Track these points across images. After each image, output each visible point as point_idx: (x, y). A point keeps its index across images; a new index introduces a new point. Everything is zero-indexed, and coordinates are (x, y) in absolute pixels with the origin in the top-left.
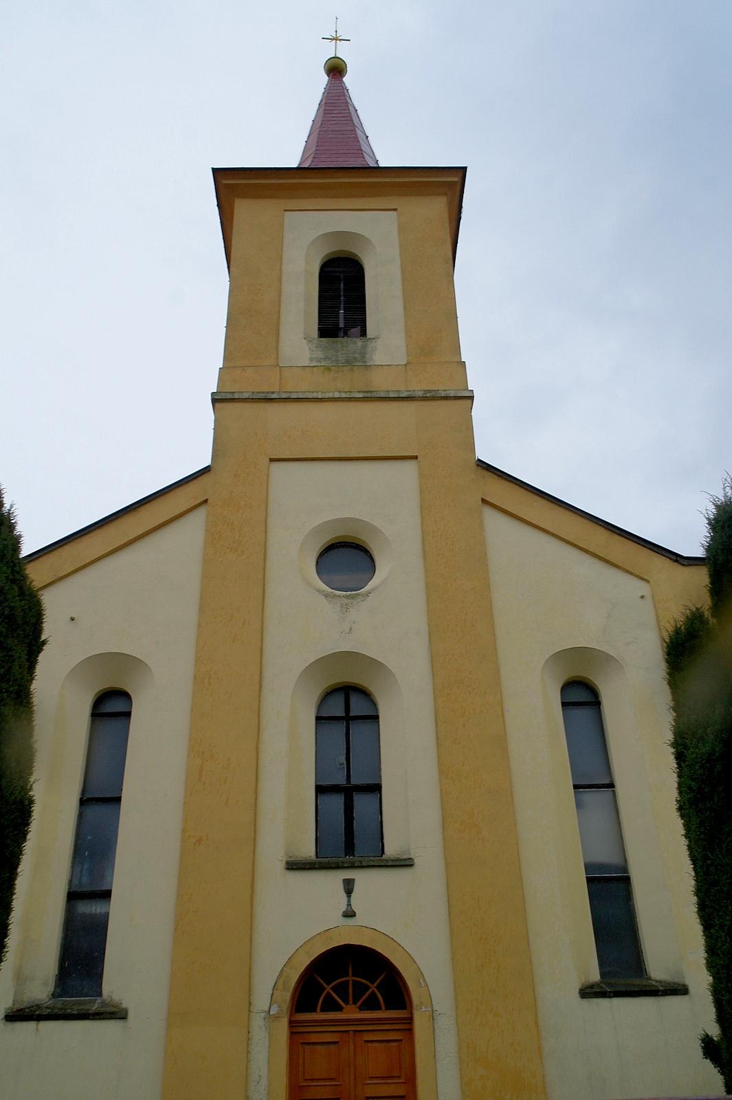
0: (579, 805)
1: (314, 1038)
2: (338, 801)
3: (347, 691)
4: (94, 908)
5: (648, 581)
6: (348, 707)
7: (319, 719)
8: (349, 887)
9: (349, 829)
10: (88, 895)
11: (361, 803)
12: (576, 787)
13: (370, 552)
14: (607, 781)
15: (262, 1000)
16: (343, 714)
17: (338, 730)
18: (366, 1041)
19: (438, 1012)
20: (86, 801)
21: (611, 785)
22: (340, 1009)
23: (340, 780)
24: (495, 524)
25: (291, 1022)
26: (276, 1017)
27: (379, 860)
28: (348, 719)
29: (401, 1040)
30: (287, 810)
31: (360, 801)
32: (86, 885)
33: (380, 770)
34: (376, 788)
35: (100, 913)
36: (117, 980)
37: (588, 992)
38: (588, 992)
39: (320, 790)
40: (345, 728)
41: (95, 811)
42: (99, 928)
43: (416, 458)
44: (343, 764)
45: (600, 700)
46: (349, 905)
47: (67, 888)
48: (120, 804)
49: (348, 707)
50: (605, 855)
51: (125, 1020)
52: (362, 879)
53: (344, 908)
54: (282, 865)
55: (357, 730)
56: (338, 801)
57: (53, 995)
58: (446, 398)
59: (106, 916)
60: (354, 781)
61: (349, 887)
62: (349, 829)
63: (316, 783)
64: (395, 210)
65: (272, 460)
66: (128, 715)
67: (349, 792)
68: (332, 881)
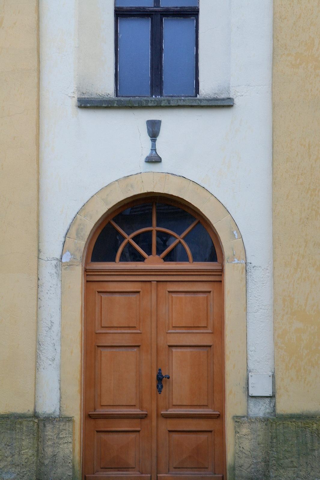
1: (112, 287)
2: (142, 29)
8: (154, 129)
15: (53, 246)
29: (210, 292)
31: (171, 29)
39: (121, 14)
46: (154, 149)
52: (172, 121)
53: (147, 152)
56: (142, 29)
61: (154, 129)
68: (135, 122)
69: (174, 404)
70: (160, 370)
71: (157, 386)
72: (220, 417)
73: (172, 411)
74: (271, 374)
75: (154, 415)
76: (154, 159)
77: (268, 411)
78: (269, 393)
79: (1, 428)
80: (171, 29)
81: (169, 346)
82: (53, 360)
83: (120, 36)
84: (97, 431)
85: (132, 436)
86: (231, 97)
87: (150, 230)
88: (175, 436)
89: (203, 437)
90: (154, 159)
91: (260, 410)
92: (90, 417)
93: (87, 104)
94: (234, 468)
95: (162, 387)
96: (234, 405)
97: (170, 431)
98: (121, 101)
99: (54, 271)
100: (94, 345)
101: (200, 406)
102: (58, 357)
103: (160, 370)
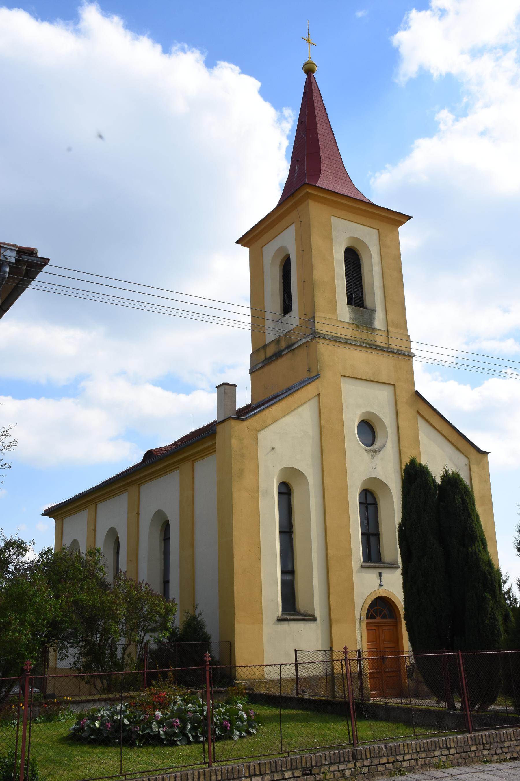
5: (468, 458)
10: (288, 570)
11: (373, 539)
15: (358, 616)
22: (375, 618)
24: (421, 423)
26: (363, 621)
36: (301, 604)
43: (394, 385)
58: (405, 355)
64: (378, 230)
65: (342, 376)
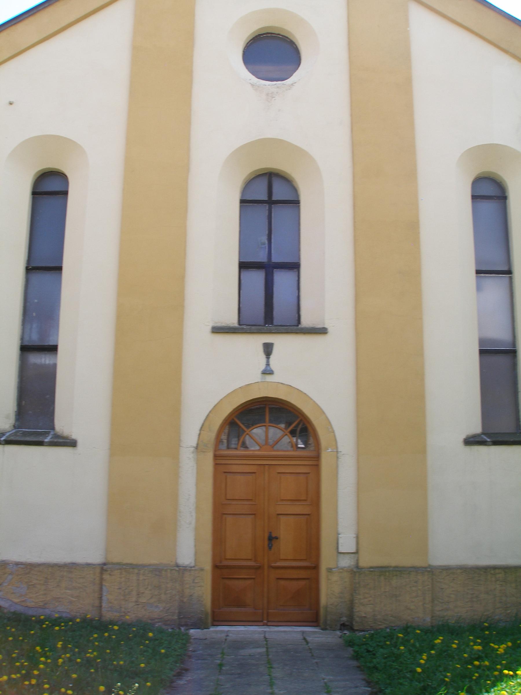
0: (479, 288)
1: (235, 469)
2: (257, 278)
3: (271, 177)
4: (44, 359)
6: (270, 197)
7: (243, 202)
8: (268, 349)
9: (269, 293)
12: (478, 272)
13: (296, 43)
14: (506, 268)
15: (190, 435)
16: (265, 197)
17: (262, 211)
18: (279, 473)
19: (342, 453)
20: (31, 269)
21: (509, 272)
23: (262, 257)
25: (216, 457)
27: (294, 326)
28: (270, 202)
29: (309, 473)
30: (213, 282)
31: (281, 279)
32: (34, 338)
33: (299, 250)
34: (294, 267)
35: (49, 364)
37: (471, 441)
38: (471, 441)
39: (243, 266)
40: (267, 211)
41: (38, 278)
42: (49, 377)
44: (264, 244)
45: (507, 194)
46: (268, 364)
47: (20, 342)
48: (61, 273)
49: (270, 197)
50: (499, 333)
51: (75, 448)
52: (283, 343)
53: (263, 367)
54: (209, 328)
55: (280, 214)
56: (257, 278)
57: (14, 427)
59: (55, 366)
60: (276, 259)
61: (268, 349)
62: (269, 293)
63: (239, 260)
66: (65, 193)
67: (269, 268)
68: (254, 343)
69: (281, 558)
70: (271, 533)
71: (269, 545)
72: (316, 568)
73: (279, 564)
74: (355, 536)
75: (266, 567)
76: (268, 372)
77: (352, 563)
78: (354, 550)
79: (109, 690)
80: (281, 279)
81: (278, 514)
82: (190, 524)
83: (242, 282)
84: (223, 578)
85: (248, 582)
86: (326, 326)
87: (267, 417)
88: (282, 582)
89: (302, 583)
90: (268, 372)
91: (346, 562)
92: (217, 567)
93: (217, 330)
94: (326, 607)
95: (272, 545)
96: (326, 560)
97: (278, 579)
98: (244, 326)
99: (191, 456)
100: (222, 510)
101: (301, 560)
102: (194, 522)
103: (271, 533)
